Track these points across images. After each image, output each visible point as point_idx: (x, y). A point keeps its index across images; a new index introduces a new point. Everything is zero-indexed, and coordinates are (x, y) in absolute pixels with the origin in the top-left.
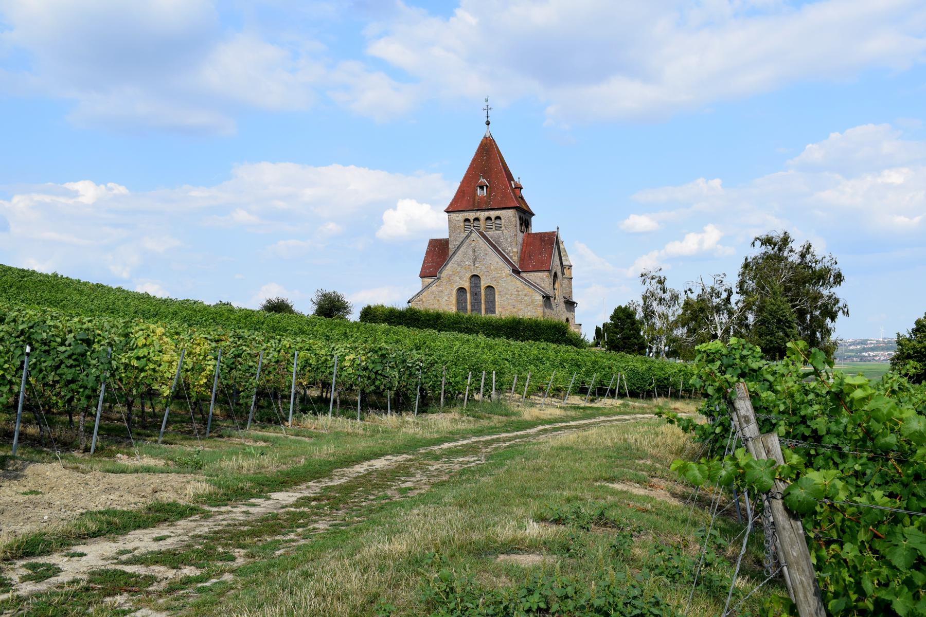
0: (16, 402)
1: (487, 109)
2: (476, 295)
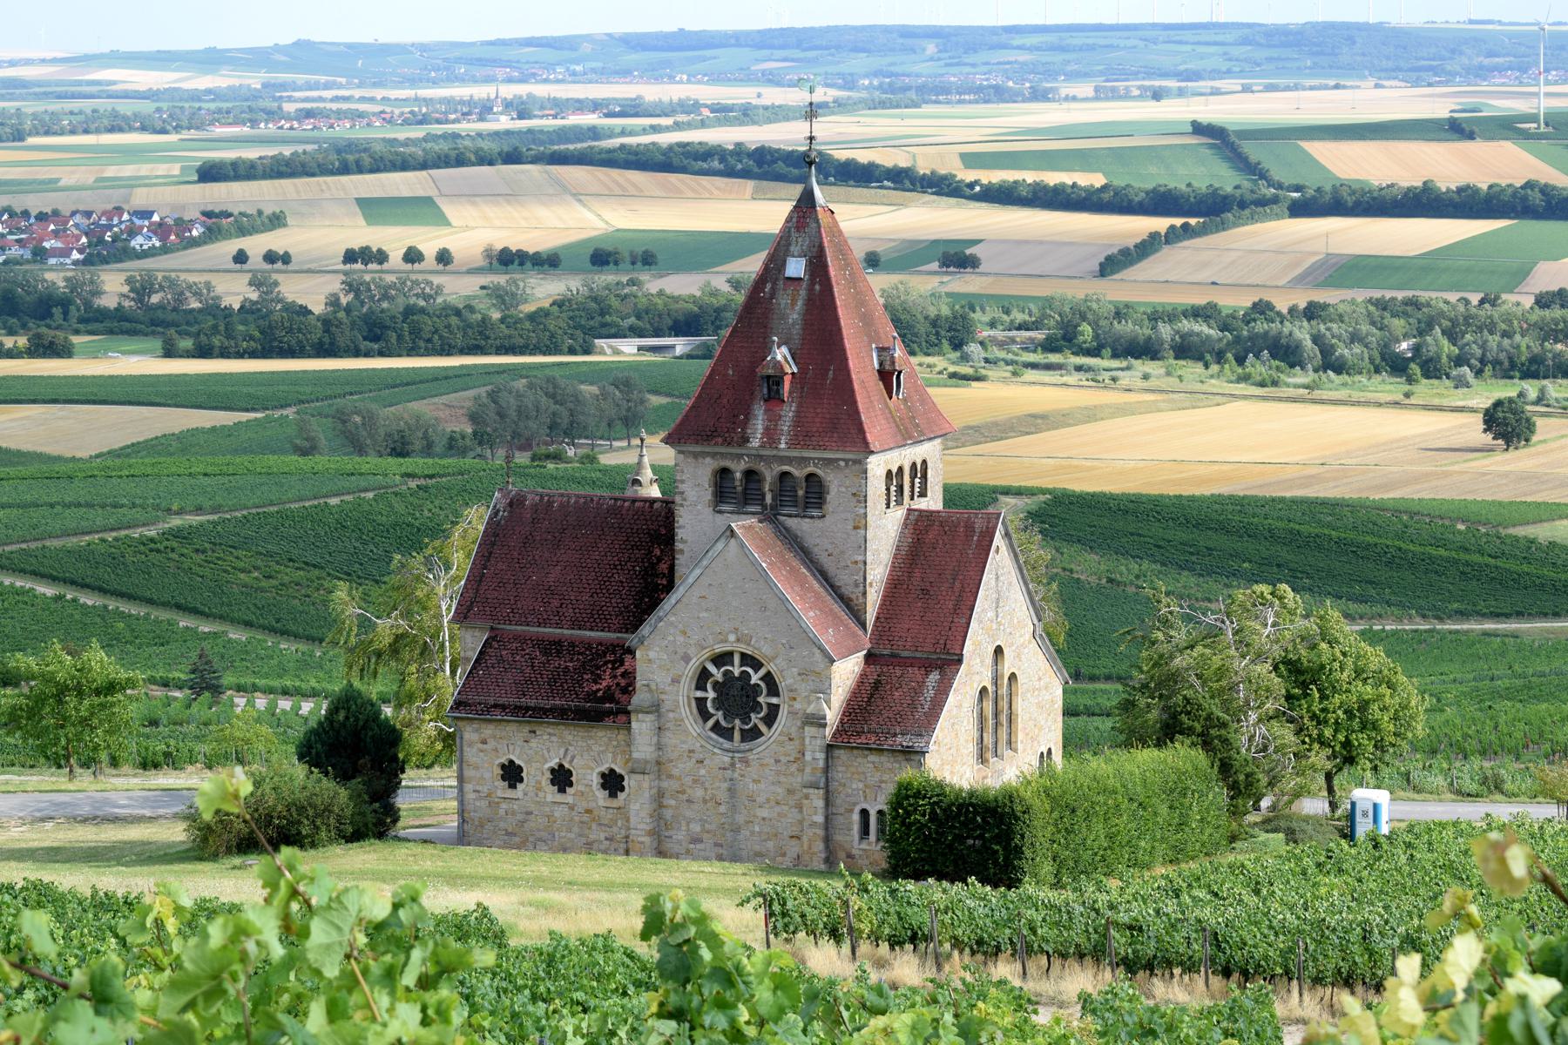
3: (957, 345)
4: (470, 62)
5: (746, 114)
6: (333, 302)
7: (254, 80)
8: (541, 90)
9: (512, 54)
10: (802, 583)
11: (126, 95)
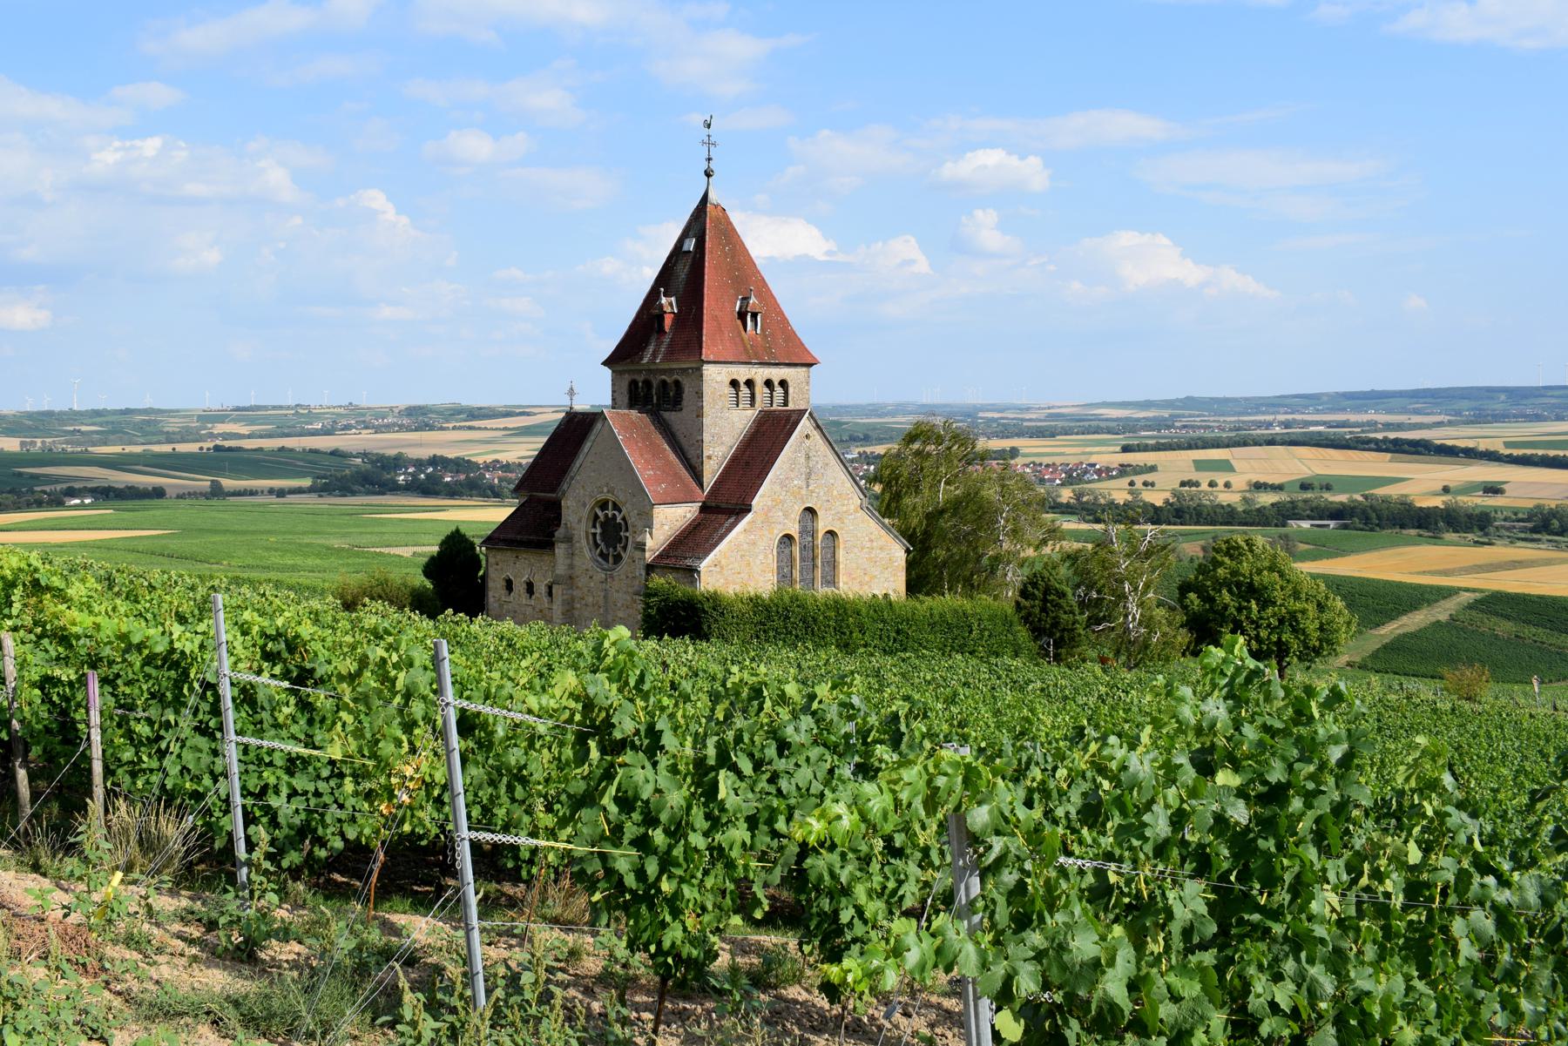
0: (315, 748)
1: (709, 143)
2: (809, 551)
3: (1482, 529)
4: (1267, 405)
5: (1399, 427)
6: (1167, 502)
7: (1166, 414)
8: (1298, 417)
9: (1288, 401)
10: (656, 453)
11: (1107, 420)
